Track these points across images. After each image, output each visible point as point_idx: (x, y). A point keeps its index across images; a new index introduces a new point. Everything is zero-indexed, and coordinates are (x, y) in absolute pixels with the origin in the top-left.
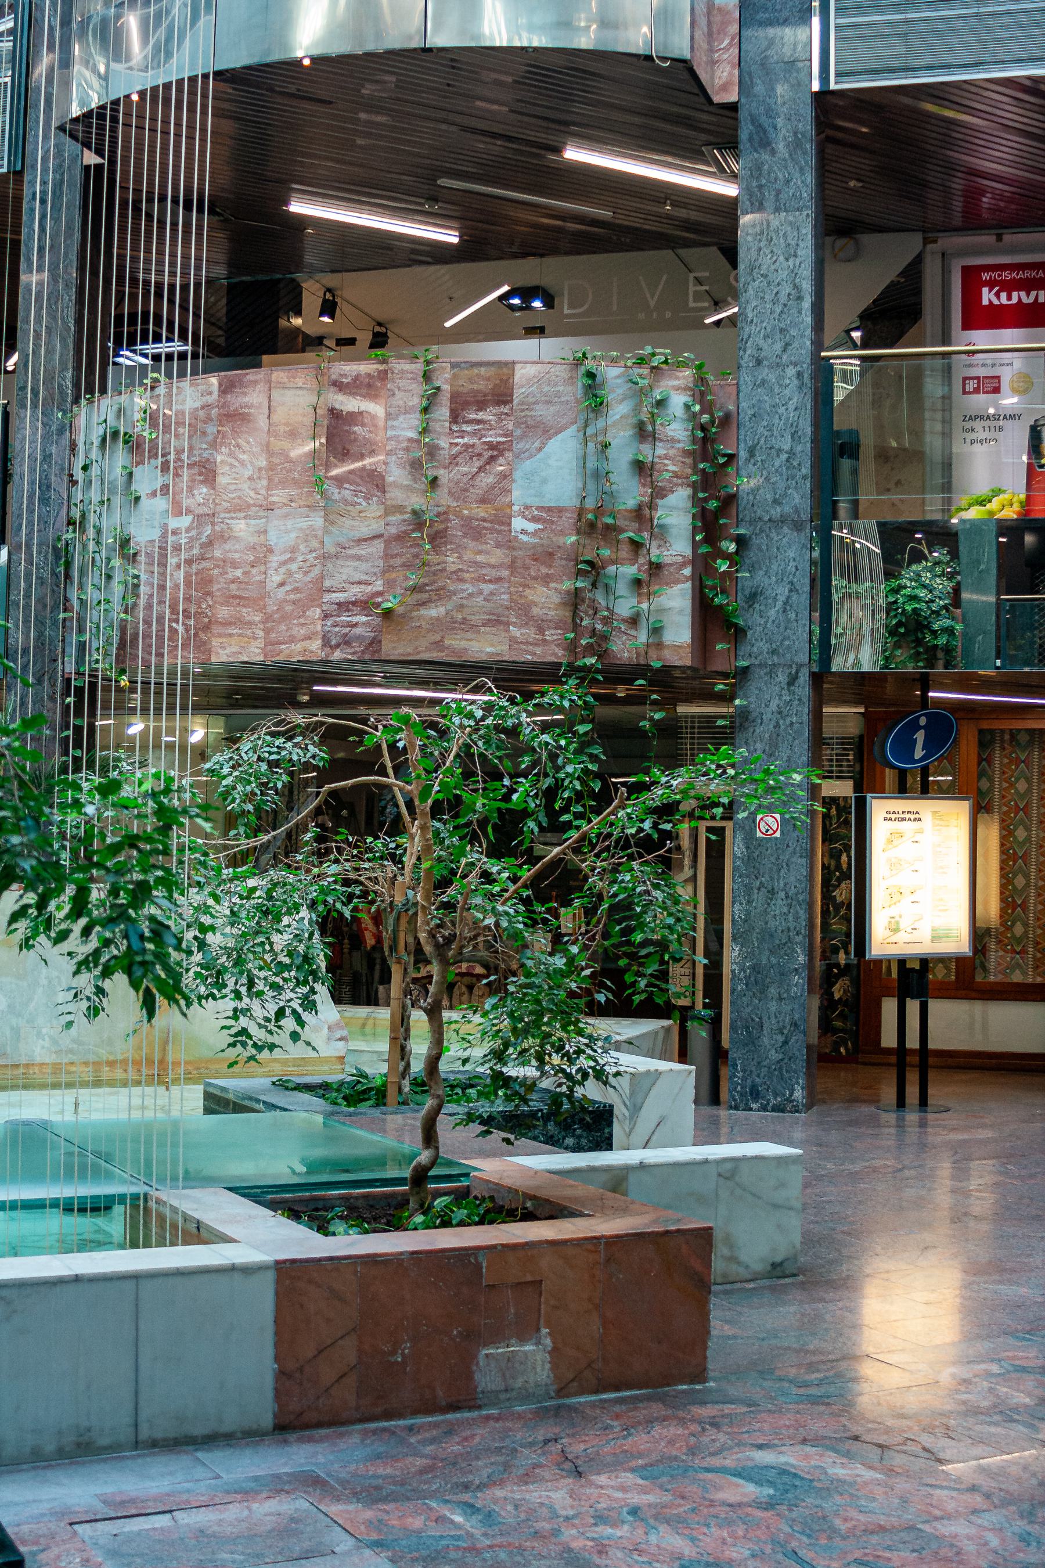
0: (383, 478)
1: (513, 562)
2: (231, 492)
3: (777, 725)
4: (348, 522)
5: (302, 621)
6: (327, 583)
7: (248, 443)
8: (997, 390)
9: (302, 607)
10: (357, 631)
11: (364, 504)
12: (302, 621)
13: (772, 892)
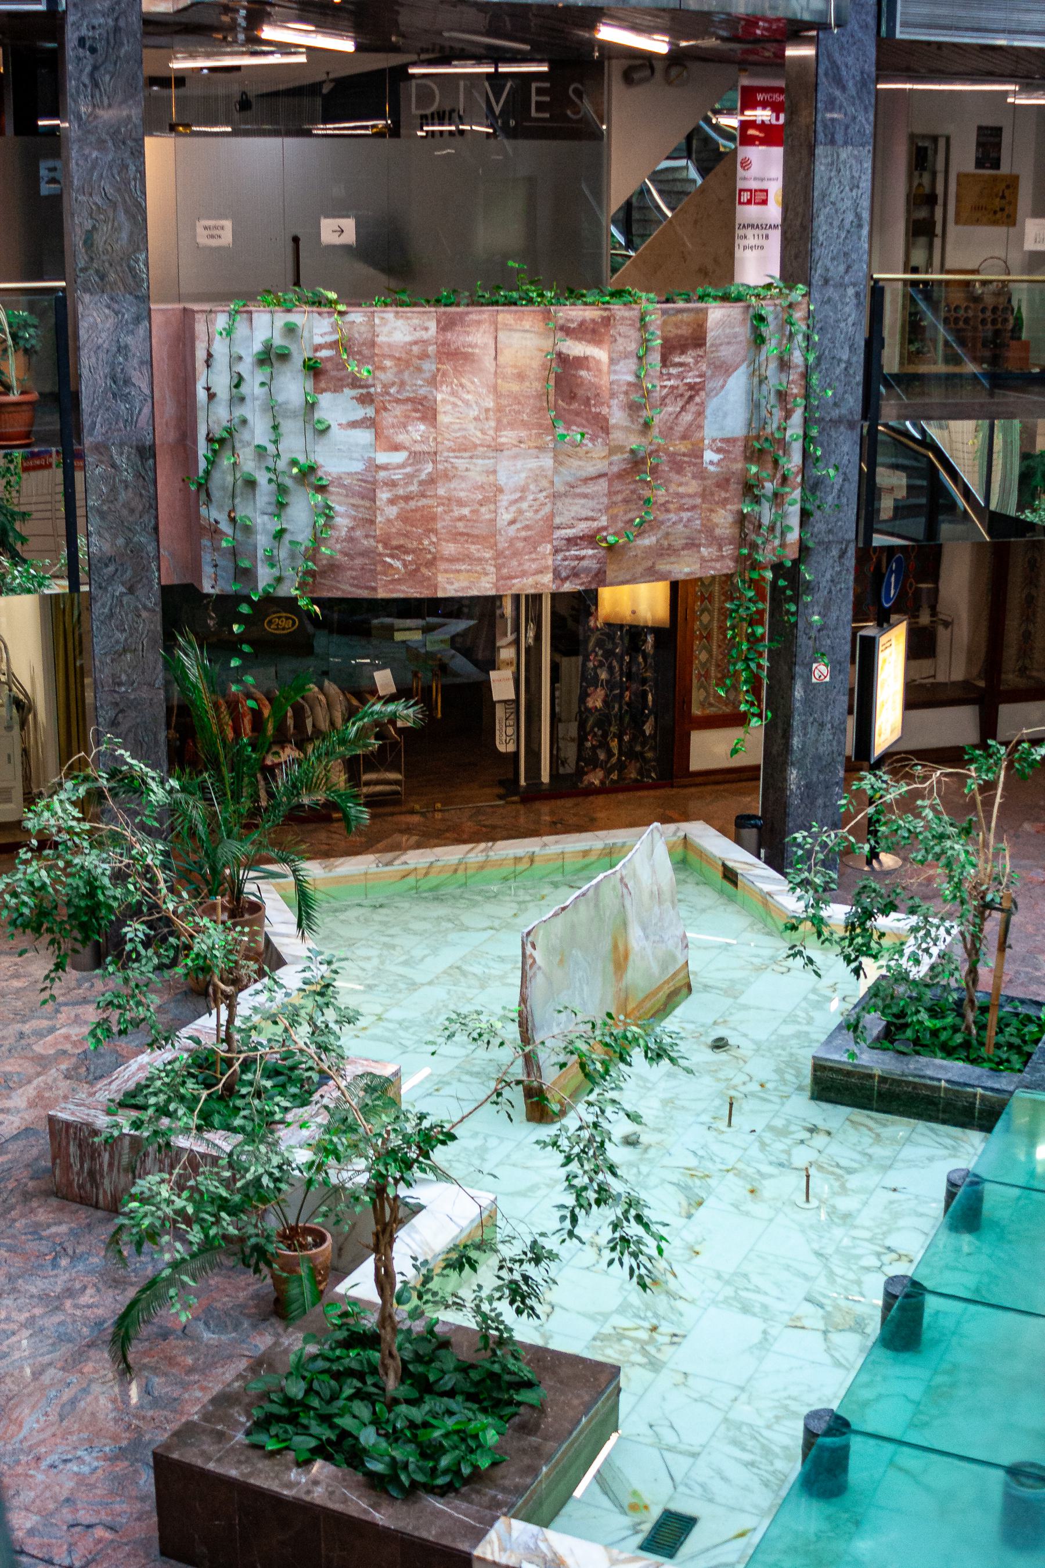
0: (607, 420)
1: (704, 490)
2: (455, 431)
3: (830, 592)
4: (575, 463)
5: (534, 556)
6: (557, 520)
7: (473, 382)
8: (764, 202)
9: (533, 543)
10: (585, 563)
11: (590, 445)
12: (534, 556)
13: (822, 725)
